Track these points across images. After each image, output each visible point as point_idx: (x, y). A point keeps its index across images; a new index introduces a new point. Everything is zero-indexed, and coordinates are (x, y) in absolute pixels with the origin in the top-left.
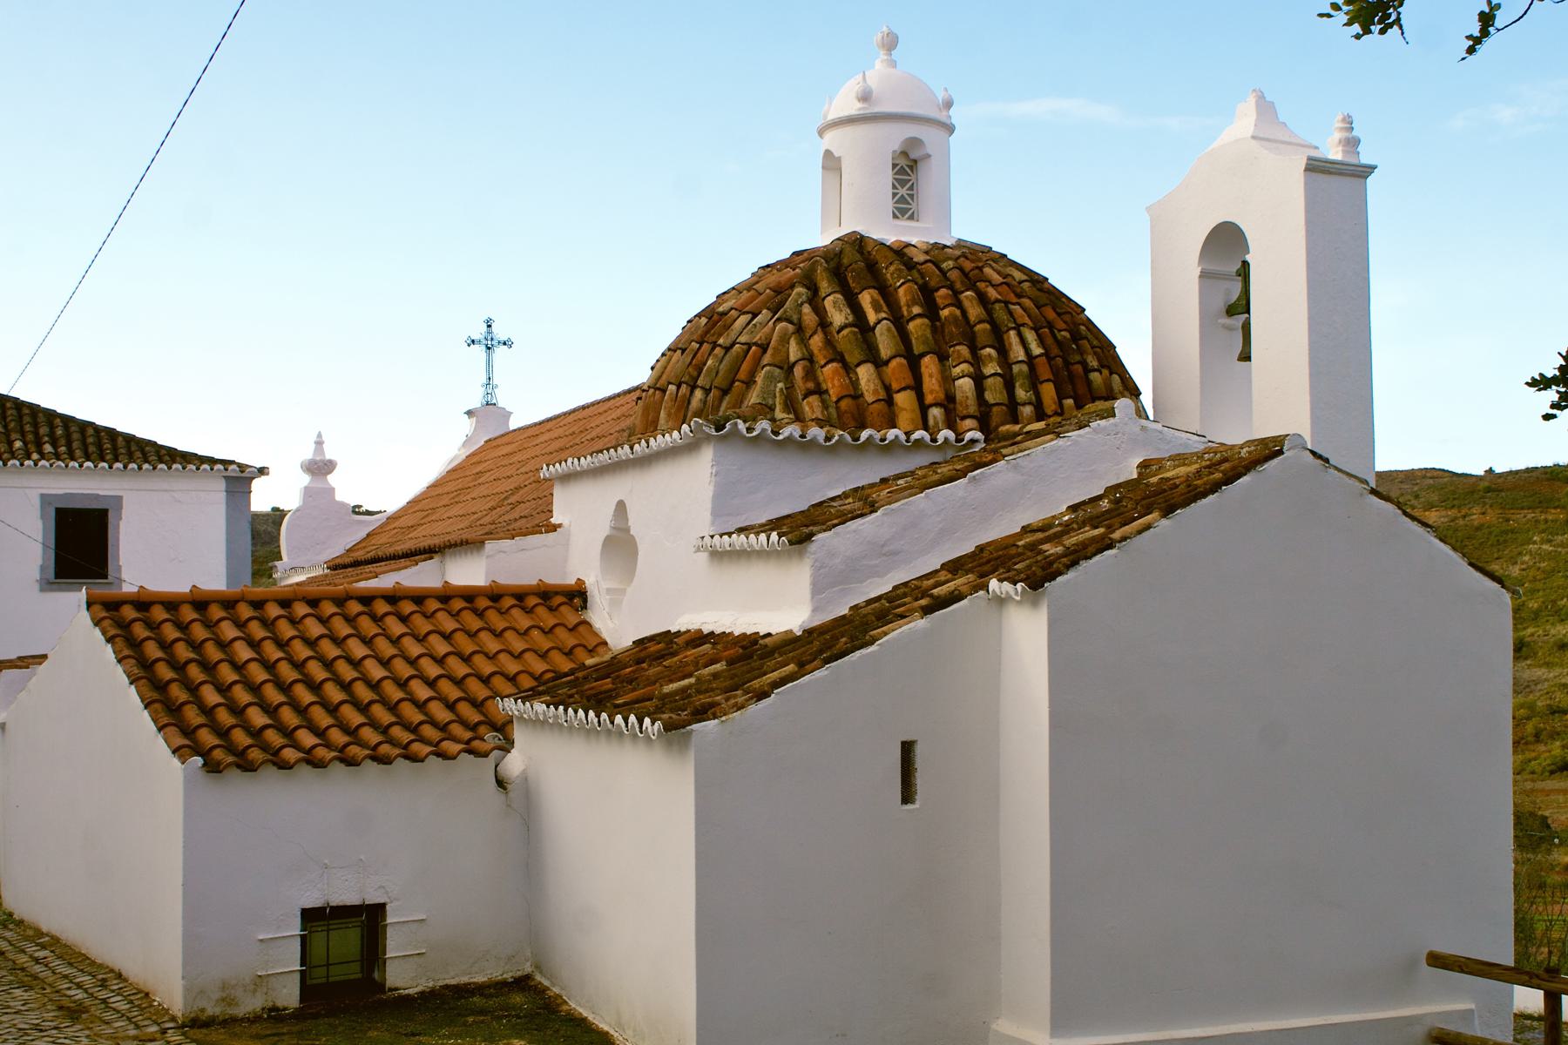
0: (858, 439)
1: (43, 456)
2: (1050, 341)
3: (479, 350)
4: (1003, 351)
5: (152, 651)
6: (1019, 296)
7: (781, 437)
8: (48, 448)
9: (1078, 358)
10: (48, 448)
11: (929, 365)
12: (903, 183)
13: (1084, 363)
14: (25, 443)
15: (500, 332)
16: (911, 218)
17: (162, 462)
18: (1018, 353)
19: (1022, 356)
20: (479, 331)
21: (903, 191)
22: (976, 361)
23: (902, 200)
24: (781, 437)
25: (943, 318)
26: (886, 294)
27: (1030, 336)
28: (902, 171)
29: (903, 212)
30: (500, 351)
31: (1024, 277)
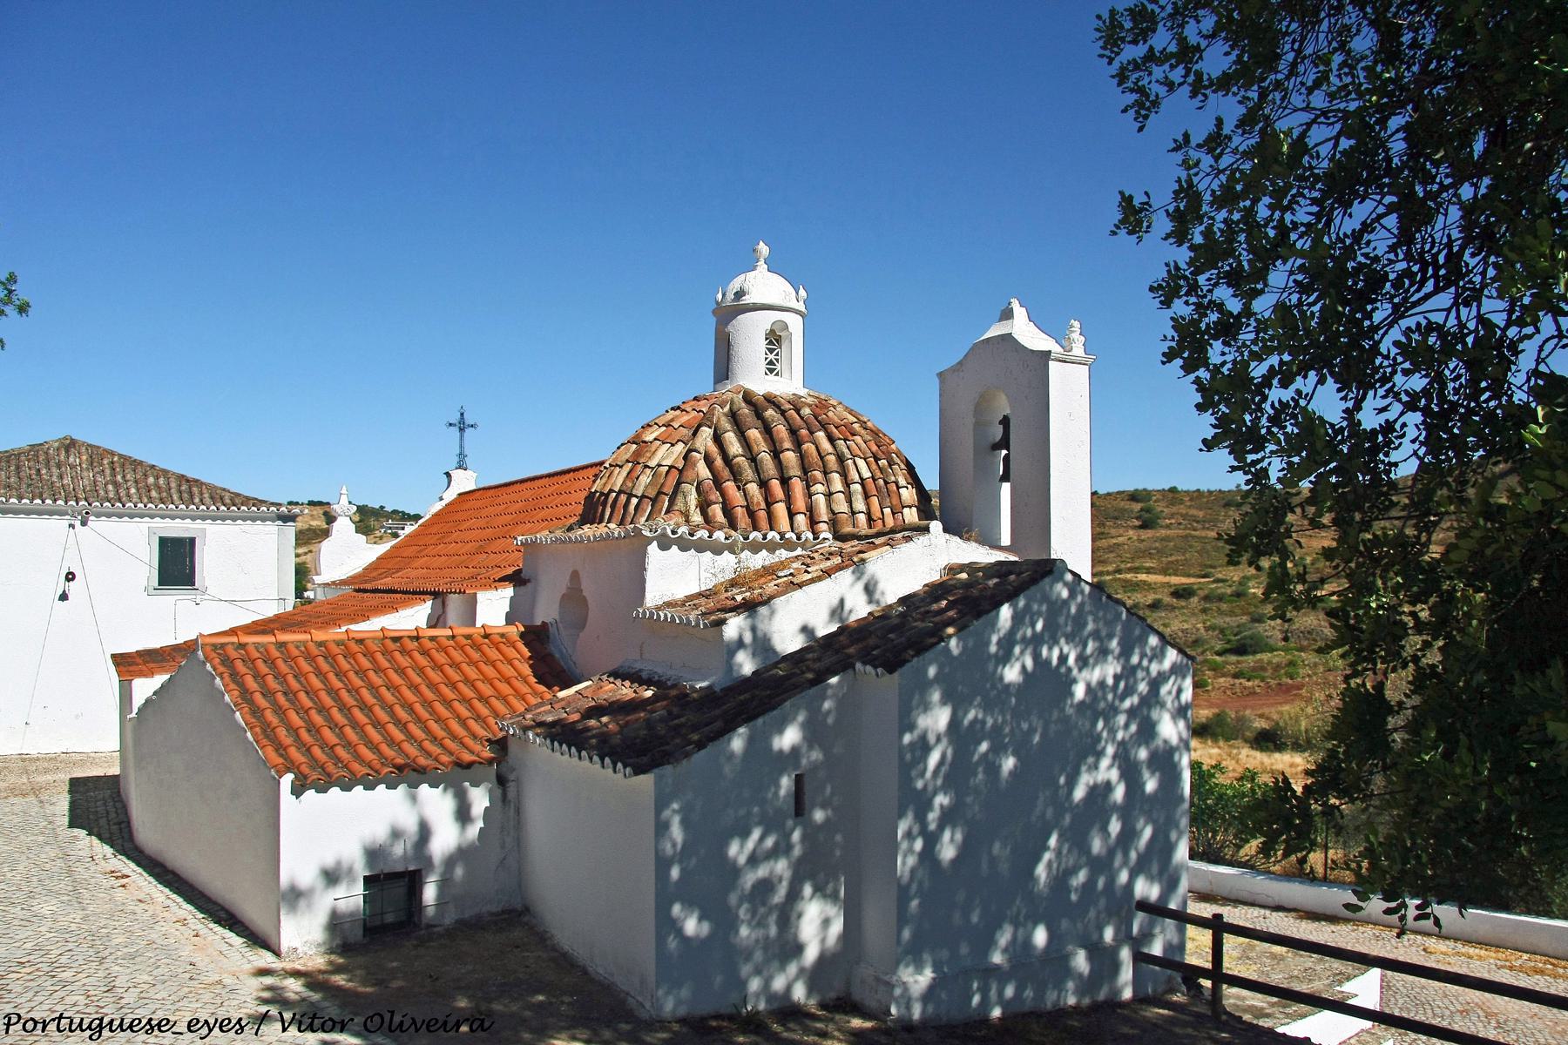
0: (748, 538)
1: (151, 500)
2: (874, 466)
3: (455, 430)
4: (844, 474)
5: (251, 683)
6: (854, 435)
7: (695, 538)
8: (154, 494)
9: (893, 479)
10: (154, 494)
11: (798, 486)
12: (771, 351)
13: (896, 483)
14: (138, 490)
15: (469, 420)
16: (777, 374)
17: (234, 505)
18: (854, 476)
19: (857, 478)
20: (455, 418)
21: (771, 357)
22: (828, 482)
23: (771, 363)
24: (695, 538)
25: (1371, 896)
26: (767, 430)
27: (861, 463)
28: (771, 343)
29: (771, 371)
30: (469, 431)
31: (855, 420)
